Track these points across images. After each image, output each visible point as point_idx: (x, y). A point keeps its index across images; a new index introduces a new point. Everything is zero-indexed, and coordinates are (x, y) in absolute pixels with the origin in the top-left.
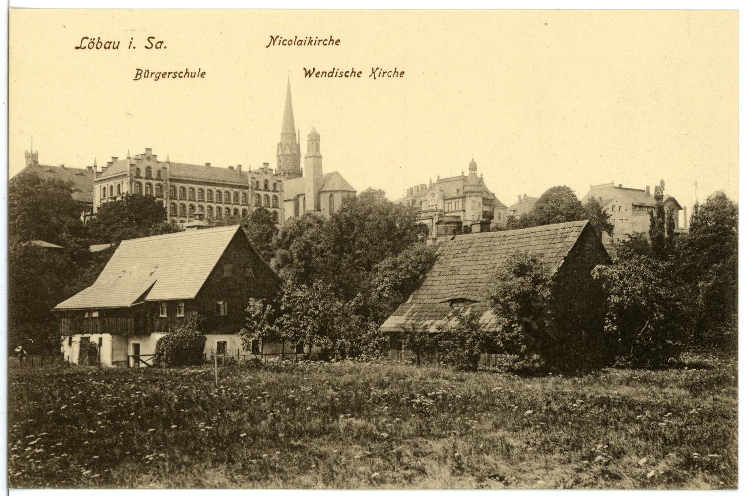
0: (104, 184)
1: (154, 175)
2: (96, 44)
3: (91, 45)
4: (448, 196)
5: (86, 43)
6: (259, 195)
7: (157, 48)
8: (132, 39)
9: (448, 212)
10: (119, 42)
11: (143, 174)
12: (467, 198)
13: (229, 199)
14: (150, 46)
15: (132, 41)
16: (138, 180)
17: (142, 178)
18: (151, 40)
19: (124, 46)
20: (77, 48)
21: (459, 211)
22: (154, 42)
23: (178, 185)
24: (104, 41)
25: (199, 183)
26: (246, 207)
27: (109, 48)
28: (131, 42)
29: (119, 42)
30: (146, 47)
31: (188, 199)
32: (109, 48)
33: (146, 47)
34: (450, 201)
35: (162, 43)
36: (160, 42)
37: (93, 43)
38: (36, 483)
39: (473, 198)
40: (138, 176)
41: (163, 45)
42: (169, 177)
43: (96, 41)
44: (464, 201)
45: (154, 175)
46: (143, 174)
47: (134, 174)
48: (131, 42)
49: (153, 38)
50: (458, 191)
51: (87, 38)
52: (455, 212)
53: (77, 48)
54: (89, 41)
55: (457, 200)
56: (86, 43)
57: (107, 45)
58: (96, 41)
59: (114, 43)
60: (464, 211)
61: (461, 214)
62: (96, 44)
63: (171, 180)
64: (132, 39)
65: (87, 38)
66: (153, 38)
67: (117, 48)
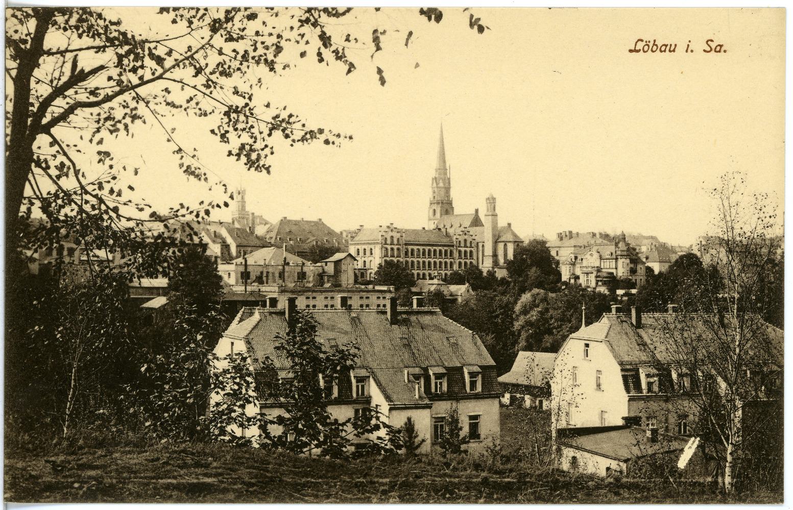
0: (359, 247)
1: (395, 242)
2: (652, 47)
3: (646, 48)
4: (604, 257)
5: (640, 46)
6: (387, 249)
7: (715, 51)
8: (690, 41)
9: (604, 268)
10: (676, 45)
11: (389, 242)
12: (619, 259)
13: (419, 255)
14: (708, 49)
15: (689, 44)
16: (385, 246)
17: (388, 244)
18: (709, 43)
19: (681, 49)
20: (631, 51)
21: (612, 269)
22: (713, 45)
23: (410, 248)
24: (659, 44)
25: (433, 245)
26: (452, 260)
27: (665, 51)
28: (688, 45)
29: (676, 45)
30: (705, 51)
31: (416, 256)
32: (665, 51)
33: (705, 51)
34: (605, 261)
35: (721, 46)
36: (719, 45)
37: (648, 45)
38: (316, 496)
39: (623, 260)
40: (386, 244)
41: (723, 49)
42: (404, 242)
43: (651, 44)
44: (616, 262)
45: (395, 242)
46: (389, 242)
47: (384, 242)
48: (688, 45)
49: (712, 41)
50: (612, 254)
51: (642, 41)
52: (610, 268)
53: (631, 51)
54: (644, 43)
55: (611, 260)
56: (640, 46)
57: (663, 48)
58: (651, 44)
59: (671, 45)
60: (616, 268)
61: (614, 271)
62: (652, 47)
63: (406, 244)
64: (690, 41)
65: (642, 41)
66: (712, 41)
67: (674, 51)
